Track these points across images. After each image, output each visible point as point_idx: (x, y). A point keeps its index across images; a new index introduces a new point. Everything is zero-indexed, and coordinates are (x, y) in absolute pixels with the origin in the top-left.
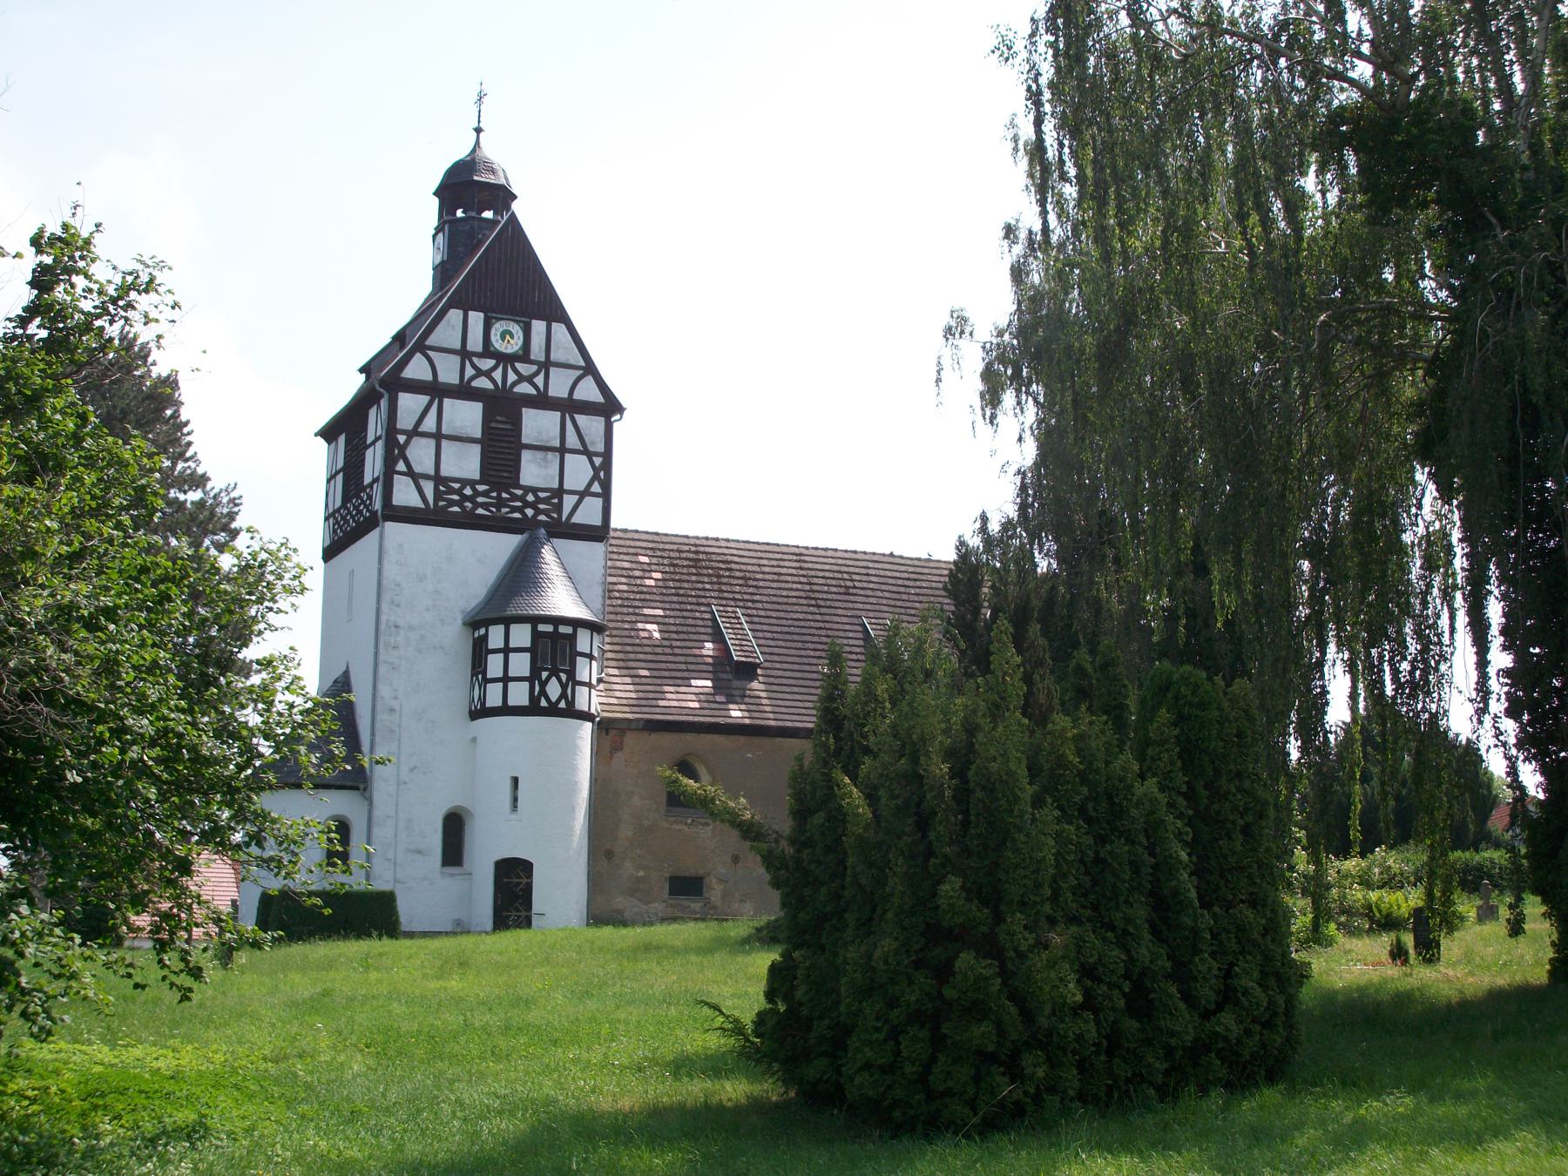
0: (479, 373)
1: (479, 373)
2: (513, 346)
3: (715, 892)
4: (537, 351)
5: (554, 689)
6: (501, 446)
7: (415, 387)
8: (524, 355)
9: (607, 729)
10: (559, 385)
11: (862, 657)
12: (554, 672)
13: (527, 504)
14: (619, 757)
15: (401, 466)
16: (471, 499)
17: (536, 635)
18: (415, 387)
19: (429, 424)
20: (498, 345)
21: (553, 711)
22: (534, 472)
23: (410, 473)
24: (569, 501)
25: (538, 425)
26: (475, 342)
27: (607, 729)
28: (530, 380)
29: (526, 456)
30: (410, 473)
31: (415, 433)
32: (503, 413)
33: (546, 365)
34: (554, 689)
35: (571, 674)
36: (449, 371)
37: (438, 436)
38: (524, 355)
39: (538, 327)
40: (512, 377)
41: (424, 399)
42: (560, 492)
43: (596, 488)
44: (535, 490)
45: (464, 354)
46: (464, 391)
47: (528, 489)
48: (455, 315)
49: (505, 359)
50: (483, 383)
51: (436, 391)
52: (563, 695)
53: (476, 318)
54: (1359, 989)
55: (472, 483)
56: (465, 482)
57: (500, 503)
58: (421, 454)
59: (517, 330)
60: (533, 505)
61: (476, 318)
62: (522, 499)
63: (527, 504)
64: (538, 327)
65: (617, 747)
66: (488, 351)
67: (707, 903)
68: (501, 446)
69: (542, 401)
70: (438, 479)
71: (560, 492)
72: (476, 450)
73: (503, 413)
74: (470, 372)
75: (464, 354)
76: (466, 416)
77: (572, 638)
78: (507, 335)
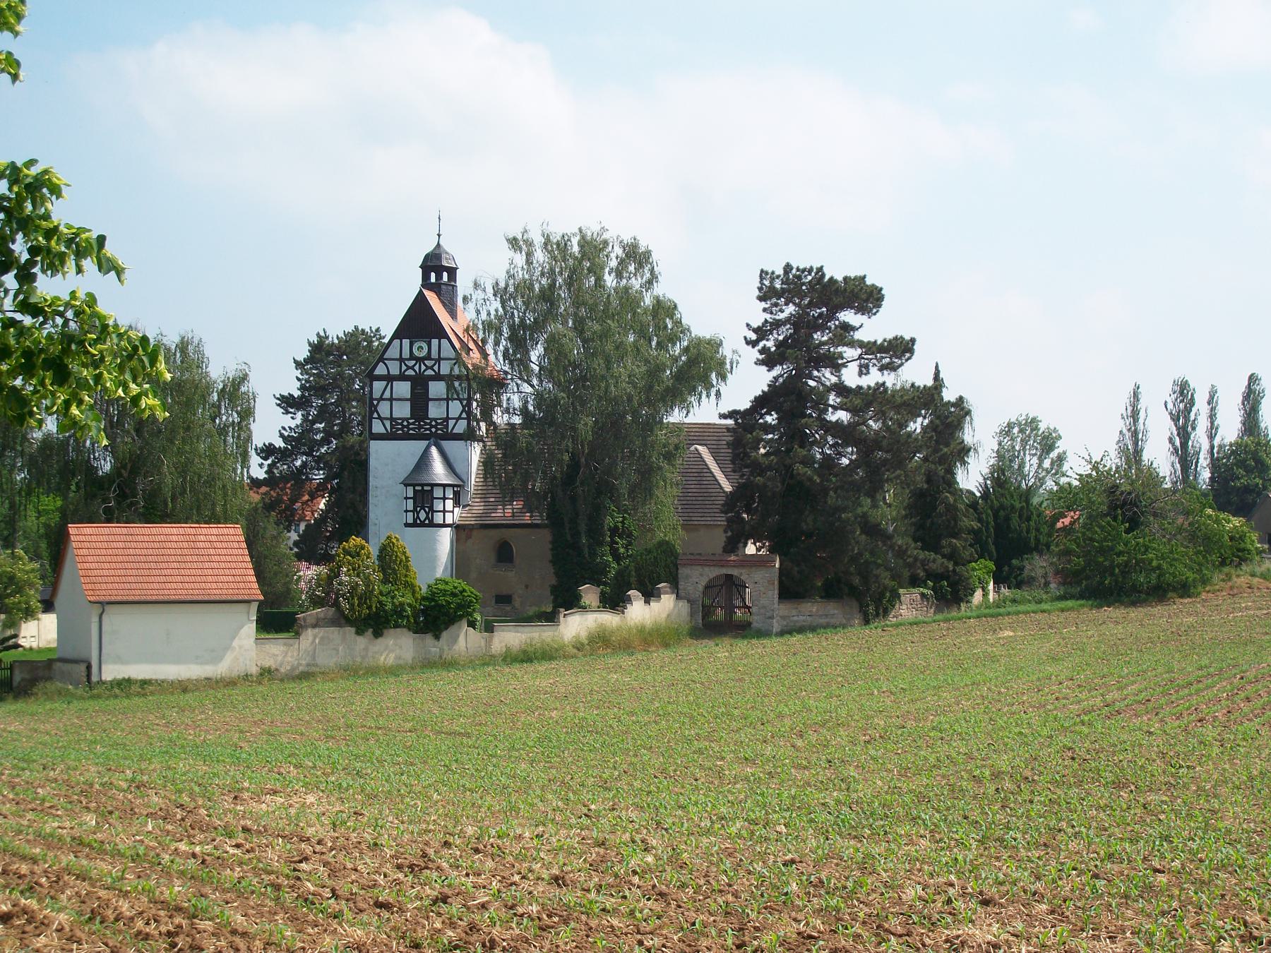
0: (408, 368)
1: (408, 368)
2: (424, 353)
3: (517, 602)
4: (434, 354)
5: (422, 515)
6: (420, 401)
7: (380, 378)
8: (428, 357)
9: (458, 528)
10: (445, 369)
11: (81, 573)
12: (423, 508)
13: (432, 426)
14: (470, 542)
15: (375, 415)
16: (407, 427)
17: (415, 491)
18: (380, 378)
19: (387, 394)
20: (416, 353)
21: (422, 525)
22: (435, 411)
23: (380, 418)
24: (451, 423)
25: (437, 389)
26: (406, 354)
27: (458, 528)
28: (431, 368)
29: (431, 404)
30: (380, 418)
31: (381, 399)
32: (420, 385)
33: (439, 360)
34: (422, 515)
35: (431, 508)
36: (394, 369)
37: (391, 400)
38: (428, 357)
39: (435, 342)
40: (423, 368)
41: (384, 383)
42: (447, 419)
43: (464, 415)
44: (435, 420)
45: (401, 360)
46: (402, 377)
47: (432, 420)
48: (397, 342)
49: (420, 360)
50: (410, 372)
51: (389, 379)
52: (427, 517)
53: (406, 342)
54: (520, 629)
55: (407, 419)
56: (403, 419)
57: (420, 427)
58: (384, 409)
59: (425, 346)
60: (435, 427)
61: (406, 342)
62: (430, 424)
63: (432, 426)
64: (435, 342)
65: (469, 537)
66: (412, 357)
67: (514, 607)
68: (420, 401)
69: (438, 377)
70: (392, 419)
71: (447, 419)
72: (408, 404)
73: (420, 385)
74: (404, 368)
75: (401, 360)
76: (403, 389)
77: (432, 490)
78: (420, 349)
